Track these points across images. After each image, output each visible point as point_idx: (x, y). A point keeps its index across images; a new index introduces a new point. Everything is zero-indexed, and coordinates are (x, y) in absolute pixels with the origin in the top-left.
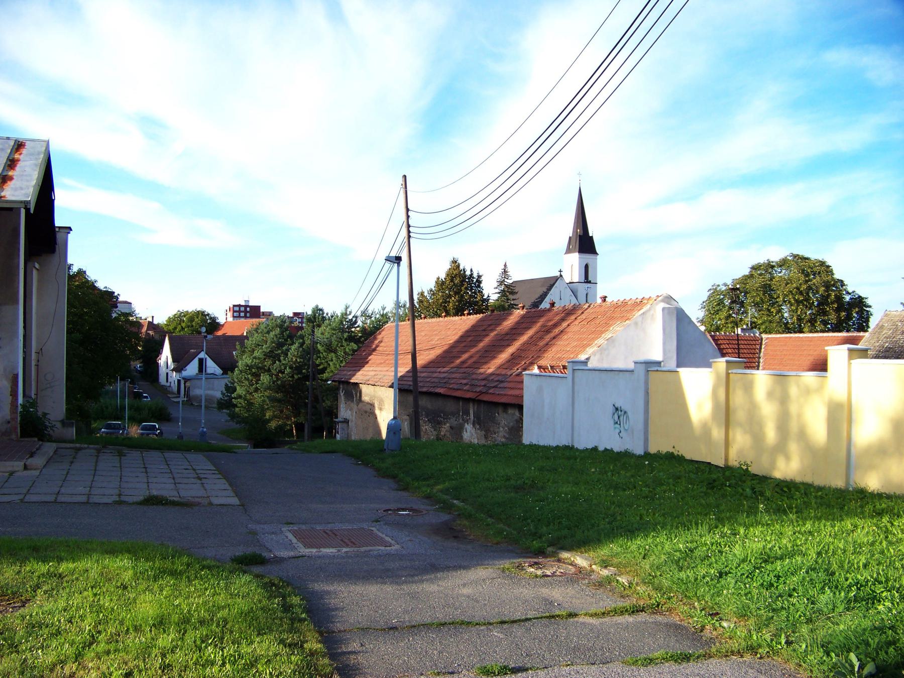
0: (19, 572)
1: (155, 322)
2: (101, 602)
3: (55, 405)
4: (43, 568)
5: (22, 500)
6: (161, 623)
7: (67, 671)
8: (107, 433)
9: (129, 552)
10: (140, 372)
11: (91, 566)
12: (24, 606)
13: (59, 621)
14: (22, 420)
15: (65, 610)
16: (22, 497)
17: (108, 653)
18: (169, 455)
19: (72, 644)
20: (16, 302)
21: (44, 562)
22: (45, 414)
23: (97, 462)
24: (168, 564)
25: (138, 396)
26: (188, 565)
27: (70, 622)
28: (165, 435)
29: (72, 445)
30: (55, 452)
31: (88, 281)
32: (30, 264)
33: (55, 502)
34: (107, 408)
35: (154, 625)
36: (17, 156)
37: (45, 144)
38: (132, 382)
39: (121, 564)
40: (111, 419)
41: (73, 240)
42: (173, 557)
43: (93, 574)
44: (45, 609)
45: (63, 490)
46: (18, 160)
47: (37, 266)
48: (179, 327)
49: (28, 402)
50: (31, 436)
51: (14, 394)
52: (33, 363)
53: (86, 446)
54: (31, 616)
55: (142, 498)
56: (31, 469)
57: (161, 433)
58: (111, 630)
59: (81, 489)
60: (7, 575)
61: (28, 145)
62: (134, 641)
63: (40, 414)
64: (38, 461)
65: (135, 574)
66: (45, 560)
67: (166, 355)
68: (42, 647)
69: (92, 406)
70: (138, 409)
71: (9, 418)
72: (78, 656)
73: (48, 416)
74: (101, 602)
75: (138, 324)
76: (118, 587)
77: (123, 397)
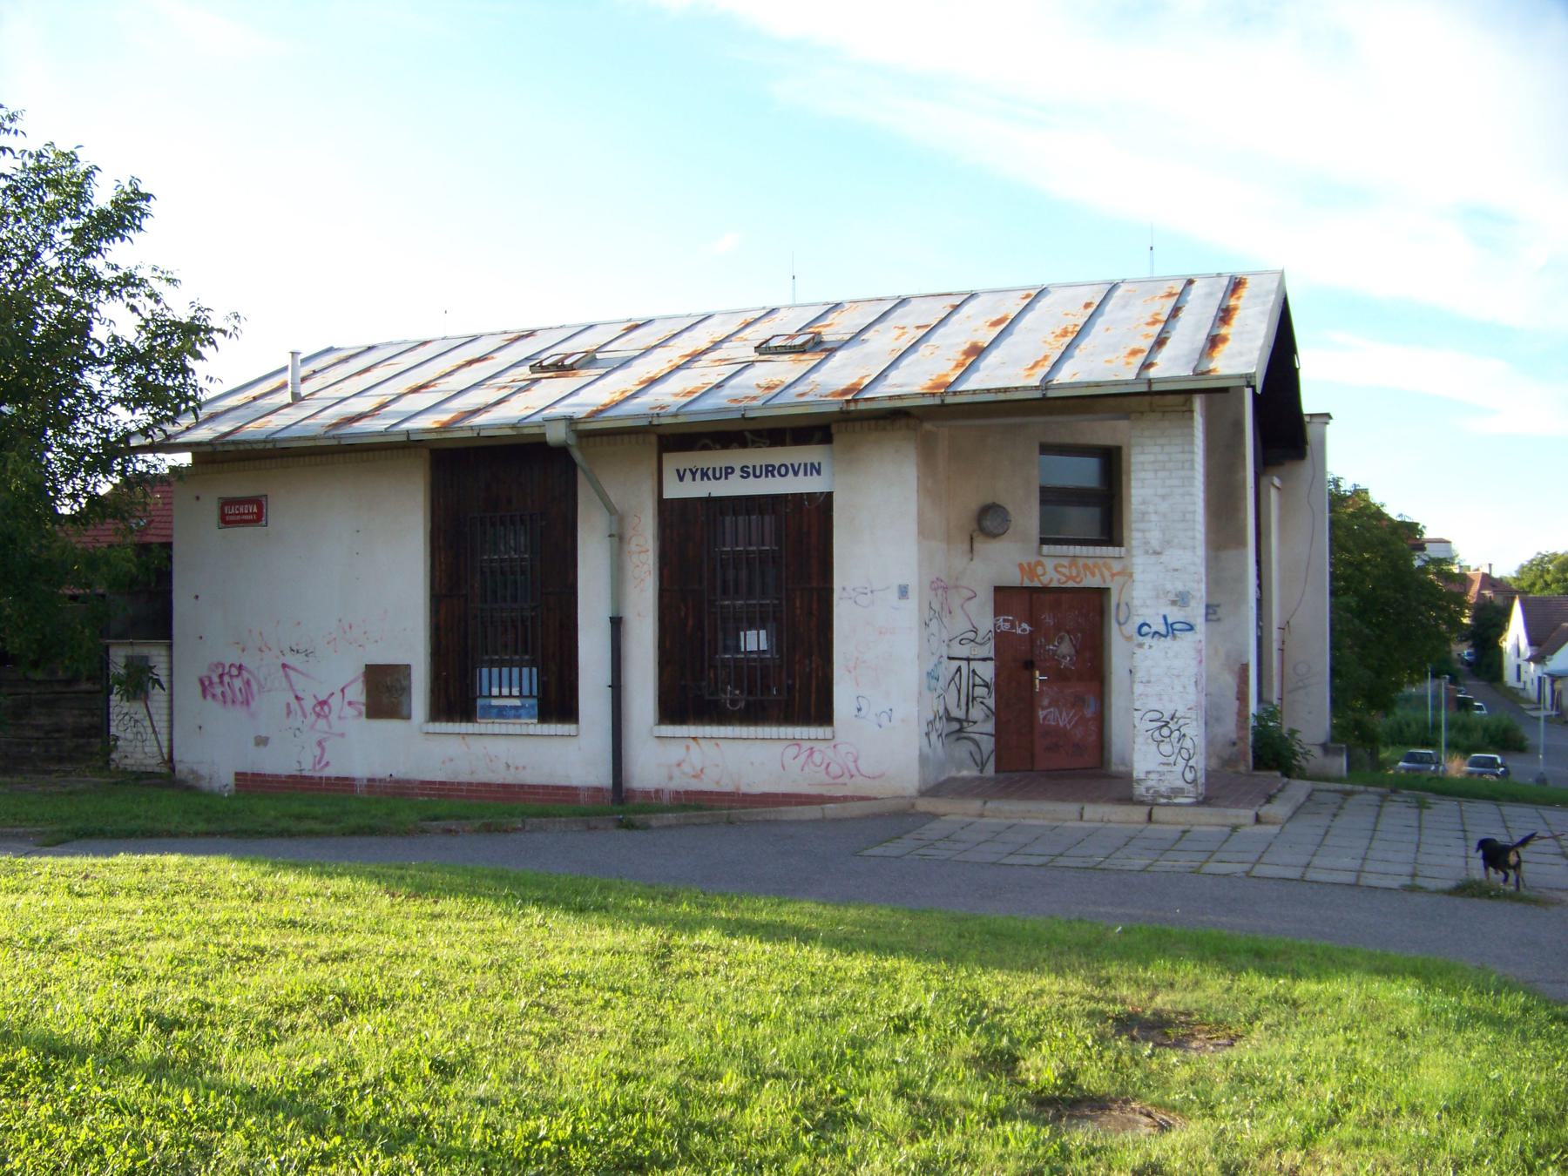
0: (1229, 989)
1: (1496, 574)
2: (1358, 1056)
3: (1311, 718)
4: (1266, 986)
5: (1247, 874)
6: (1461, 1106)
7: (1286, 1162)
8: (1408, 770)
9: (1416, 973)
10: (1469, 664)
11: (1348, 990)
12: (1231, 1045)
13: (1284, 1077)
14: (1256, 741)
15: (1295, 1061)
16: (1246, 867)
17: (1358, 1143)
18: (1508, 809)
19: (1300, 1117)
20: (1242, 543)
21: (1269, 976)
22: (1293, 732)
23: (1378, 815)
24: (1486, 1003)
25: (1464, 705)
26: (1525, 1010)
27: (1302, 1081)
28: (1511, 777)
29: (1337, 786)
30: (1309, 797)
31: (1369, 505)
32: (1264, 481)
33: (1302, 880)
34: (1408, 725)
35: (1447, 1109)
36: (1232, 302)
37: (1276, 278)
38: (1454, 680)
39: (1400, 994)
40: (1415, 744)
41: (1332, 432)
42: (1498, 992)
43: (1351, 1005)
44: (1263, 1054)
45: (1316, 861)
46: (1235, 309)
47: (1276, 481)
48: (1540, 584)
49: (1265, 710)
50: (1270, 768)
51: (1242, 697)
52: (1275, 646)
53: (1362, 788)
54: (1240, 1062)
55: (1451, 884)
56: (1267, 823)
57: (1506, 773)
58: (1369, 1104)
59: (1346, 862)
60: (1210, 992)
61: (1250, 281)
62: (1409, 1131)
63: (1285, 731)
64: (1278, 810)
65: (1424, 1014)
66: (1270, 975)
67: (1515, 636)
68: (1251, 1116)
69: (1380, 723)
70: (1464, 729)
71: (1234, 736)
72: (1307, 1141)
73: (1298, 736)
74: (1358, 1056)
75: (1463, 580)
76: (1390, 1034)
77: (1436, 708)
